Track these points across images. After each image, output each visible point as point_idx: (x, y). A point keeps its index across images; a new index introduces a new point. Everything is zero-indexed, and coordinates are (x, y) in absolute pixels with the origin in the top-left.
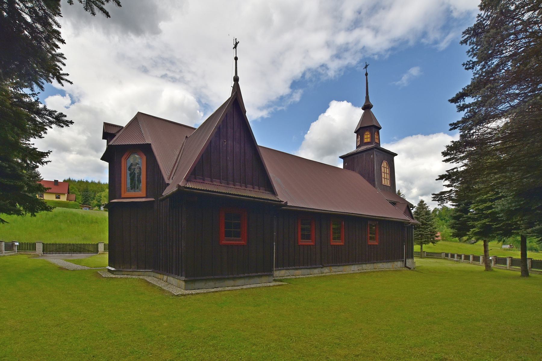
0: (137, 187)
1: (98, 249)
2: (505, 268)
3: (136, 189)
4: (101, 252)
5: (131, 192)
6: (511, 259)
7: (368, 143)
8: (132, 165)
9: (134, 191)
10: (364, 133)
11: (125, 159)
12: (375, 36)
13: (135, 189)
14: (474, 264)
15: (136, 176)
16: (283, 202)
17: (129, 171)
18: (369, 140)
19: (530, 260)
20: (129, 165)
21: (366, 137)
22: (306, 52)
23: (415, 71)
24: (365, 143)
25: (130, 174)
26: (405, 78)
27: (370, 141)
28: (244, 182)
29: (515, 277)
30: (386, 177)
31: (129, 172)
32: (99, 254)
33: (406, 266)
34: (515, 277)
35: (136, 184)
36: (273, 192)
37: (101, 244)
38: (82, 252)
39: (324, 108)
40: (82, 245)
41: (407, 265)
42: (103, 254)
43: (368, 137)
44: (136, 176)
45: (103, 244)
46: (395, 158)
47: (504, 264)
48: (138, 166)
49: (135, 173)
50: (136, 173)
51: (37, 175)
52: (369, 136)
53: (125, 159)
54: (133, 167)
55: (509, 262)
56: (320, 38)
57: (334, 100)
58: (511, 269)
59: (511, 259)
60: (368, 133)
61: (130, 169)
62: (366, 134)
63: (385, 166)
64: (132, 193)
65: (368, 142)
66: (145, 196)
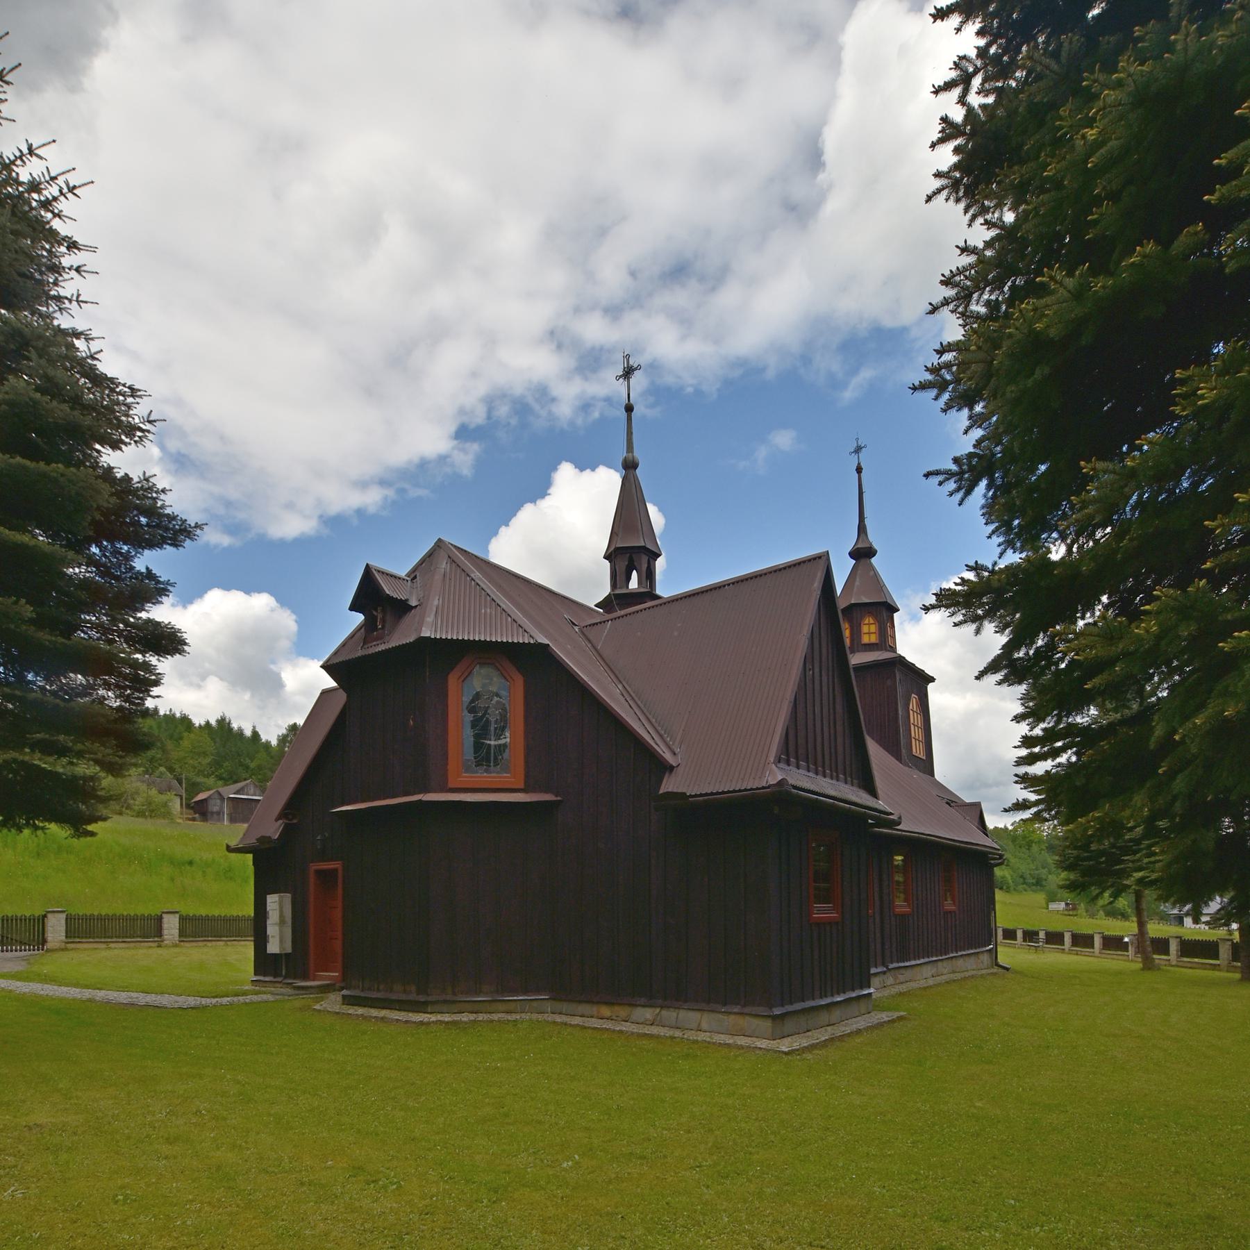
0: (496, 758)
1: (43, 934)
2: (1167, 963)
3: (492, 764)
4: (57, 945)
5: (477, 772)
6: (1179, 940)
7: (870, 647)
8: (477, 696)
9: (486, 771)
10: (862, 618)
11: (459, 679)
12: (684, 338)
13: (490, 766)
14: (1077, 954)
15: (492, 728)
16: (891, 814)
17: (469, 712)
18: (873, 639)
19: (1230, 943)
20: (466, 699)
21: (865, 629)
22: (490, 340)
23: (784, 439)
24: (865, 645)
25: (474, 725)
26: (762, 453)
27: (877, 642)
28: (834, 772)
29: (1230, 983)
30: (917, 737)
31: (469, 718)
32: (48, 951)
33: (998, 965)
34: (1230, 983)
35: (492, 755)
36: (873, 792)
37: (56, 915)
38: (29, 945)
39: (539, 489)
40: (34, 920)
41: (1001, 960)
42: (63, 950)
43: (867, 635)
44: (492, 728)
45: (177, 916)
46: (930, 687)
47: (1165, 955)
48: (498, 702)
49: (488, 721)
50: (493, 720)
51: (148, 708)
52: (873, 628)
53: (459, 679)
54: (481, 704)
55: (1175, 948)
56: (538, 315)
57: (552, 474)
58: (1180, 964)
59: (1179, 940)
60: (872, 621)
61: (472, 710)
62: (866, 622)
63: (915, 709)
64: (482, 776)
65: (873, 644)
66: (522, 786)
